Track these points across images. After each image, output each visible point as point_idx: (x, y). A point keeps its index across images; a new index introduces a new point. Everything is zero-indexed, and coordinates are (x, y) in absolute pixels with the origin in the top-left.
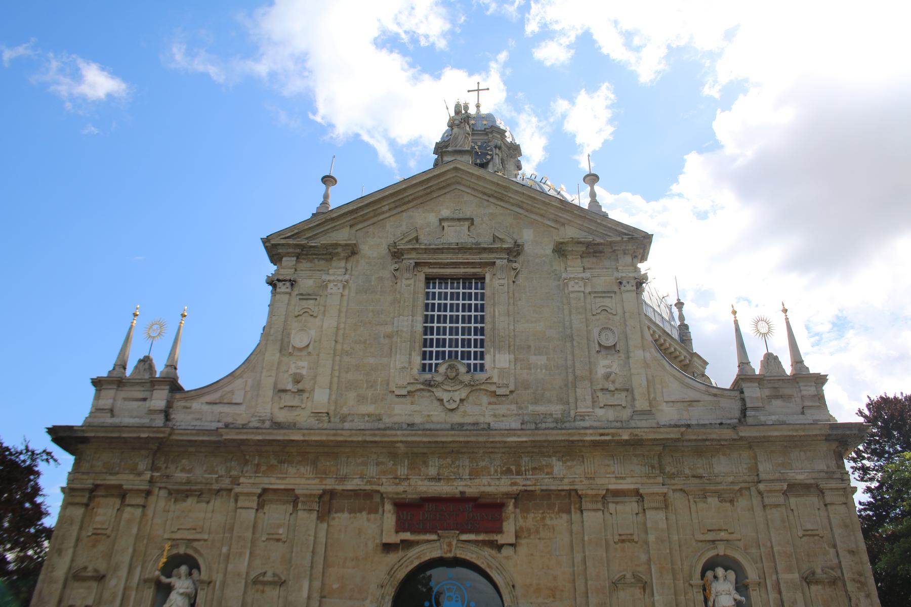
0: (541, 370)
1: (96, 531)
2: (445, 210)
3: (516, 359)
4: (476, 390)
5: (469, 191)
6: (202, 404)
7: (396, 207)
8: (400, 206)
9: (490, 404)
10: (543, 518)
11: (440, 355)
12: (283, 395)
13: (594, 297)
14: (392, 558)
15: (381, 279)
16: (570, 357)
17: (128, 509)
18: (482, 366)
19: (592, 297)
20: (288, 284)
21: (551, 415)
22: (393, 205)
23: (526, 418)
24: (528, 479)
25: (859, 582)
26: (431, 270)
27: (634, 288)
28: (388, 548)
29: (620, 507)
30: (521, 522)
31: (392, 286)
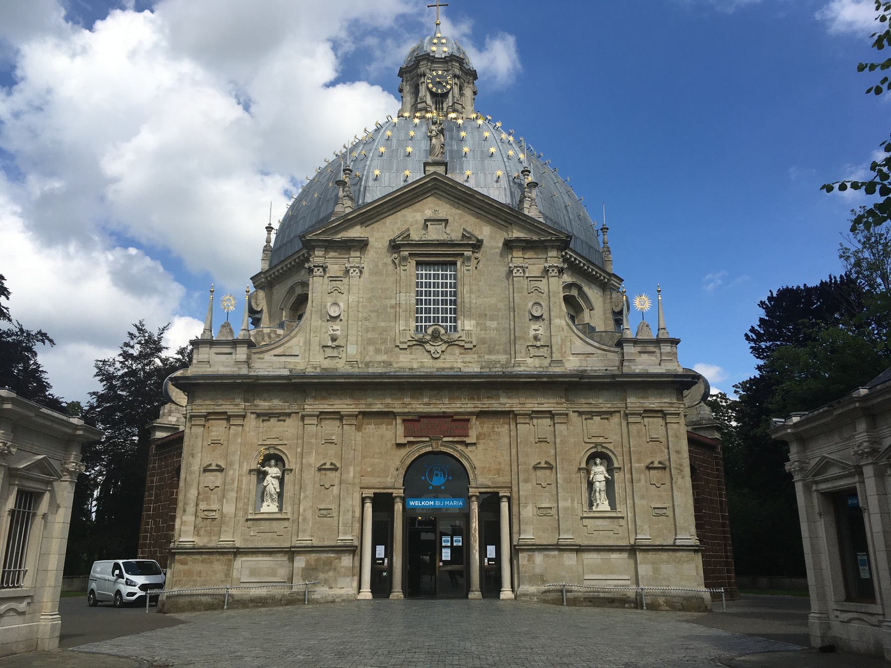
0: (494, 331)
1: (213, 442)
2: (428, 211)
3: (477, 324)
4: (451, 345)
5: (444, 195)
6: (271, 355)
7: (393, 208)
8: (395, 208)
9: (460, 354)
10: (493, 428)
11: (428, 319)
12: (326, 349)
13: (586, 419)
14: (403, 452)
15: (385, 264)
16: (512, 323)
17: (233, 427)
18: (455, 327)
19: (584, 418)
20: (321, 270)
21: (499, 362)
22: (391, 208)
23: (484, 364)
24: (485, 404)
25: (679, 469)
26: (420, 259)
27: (557, 274)
28: (399, 446)
29: (540, 421)
30: (480, 430)
31: (394, 270)
